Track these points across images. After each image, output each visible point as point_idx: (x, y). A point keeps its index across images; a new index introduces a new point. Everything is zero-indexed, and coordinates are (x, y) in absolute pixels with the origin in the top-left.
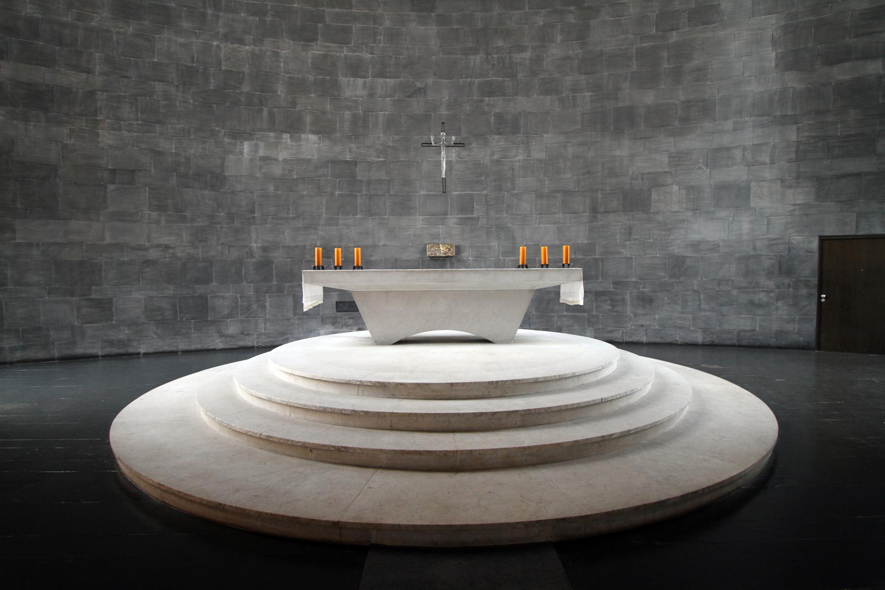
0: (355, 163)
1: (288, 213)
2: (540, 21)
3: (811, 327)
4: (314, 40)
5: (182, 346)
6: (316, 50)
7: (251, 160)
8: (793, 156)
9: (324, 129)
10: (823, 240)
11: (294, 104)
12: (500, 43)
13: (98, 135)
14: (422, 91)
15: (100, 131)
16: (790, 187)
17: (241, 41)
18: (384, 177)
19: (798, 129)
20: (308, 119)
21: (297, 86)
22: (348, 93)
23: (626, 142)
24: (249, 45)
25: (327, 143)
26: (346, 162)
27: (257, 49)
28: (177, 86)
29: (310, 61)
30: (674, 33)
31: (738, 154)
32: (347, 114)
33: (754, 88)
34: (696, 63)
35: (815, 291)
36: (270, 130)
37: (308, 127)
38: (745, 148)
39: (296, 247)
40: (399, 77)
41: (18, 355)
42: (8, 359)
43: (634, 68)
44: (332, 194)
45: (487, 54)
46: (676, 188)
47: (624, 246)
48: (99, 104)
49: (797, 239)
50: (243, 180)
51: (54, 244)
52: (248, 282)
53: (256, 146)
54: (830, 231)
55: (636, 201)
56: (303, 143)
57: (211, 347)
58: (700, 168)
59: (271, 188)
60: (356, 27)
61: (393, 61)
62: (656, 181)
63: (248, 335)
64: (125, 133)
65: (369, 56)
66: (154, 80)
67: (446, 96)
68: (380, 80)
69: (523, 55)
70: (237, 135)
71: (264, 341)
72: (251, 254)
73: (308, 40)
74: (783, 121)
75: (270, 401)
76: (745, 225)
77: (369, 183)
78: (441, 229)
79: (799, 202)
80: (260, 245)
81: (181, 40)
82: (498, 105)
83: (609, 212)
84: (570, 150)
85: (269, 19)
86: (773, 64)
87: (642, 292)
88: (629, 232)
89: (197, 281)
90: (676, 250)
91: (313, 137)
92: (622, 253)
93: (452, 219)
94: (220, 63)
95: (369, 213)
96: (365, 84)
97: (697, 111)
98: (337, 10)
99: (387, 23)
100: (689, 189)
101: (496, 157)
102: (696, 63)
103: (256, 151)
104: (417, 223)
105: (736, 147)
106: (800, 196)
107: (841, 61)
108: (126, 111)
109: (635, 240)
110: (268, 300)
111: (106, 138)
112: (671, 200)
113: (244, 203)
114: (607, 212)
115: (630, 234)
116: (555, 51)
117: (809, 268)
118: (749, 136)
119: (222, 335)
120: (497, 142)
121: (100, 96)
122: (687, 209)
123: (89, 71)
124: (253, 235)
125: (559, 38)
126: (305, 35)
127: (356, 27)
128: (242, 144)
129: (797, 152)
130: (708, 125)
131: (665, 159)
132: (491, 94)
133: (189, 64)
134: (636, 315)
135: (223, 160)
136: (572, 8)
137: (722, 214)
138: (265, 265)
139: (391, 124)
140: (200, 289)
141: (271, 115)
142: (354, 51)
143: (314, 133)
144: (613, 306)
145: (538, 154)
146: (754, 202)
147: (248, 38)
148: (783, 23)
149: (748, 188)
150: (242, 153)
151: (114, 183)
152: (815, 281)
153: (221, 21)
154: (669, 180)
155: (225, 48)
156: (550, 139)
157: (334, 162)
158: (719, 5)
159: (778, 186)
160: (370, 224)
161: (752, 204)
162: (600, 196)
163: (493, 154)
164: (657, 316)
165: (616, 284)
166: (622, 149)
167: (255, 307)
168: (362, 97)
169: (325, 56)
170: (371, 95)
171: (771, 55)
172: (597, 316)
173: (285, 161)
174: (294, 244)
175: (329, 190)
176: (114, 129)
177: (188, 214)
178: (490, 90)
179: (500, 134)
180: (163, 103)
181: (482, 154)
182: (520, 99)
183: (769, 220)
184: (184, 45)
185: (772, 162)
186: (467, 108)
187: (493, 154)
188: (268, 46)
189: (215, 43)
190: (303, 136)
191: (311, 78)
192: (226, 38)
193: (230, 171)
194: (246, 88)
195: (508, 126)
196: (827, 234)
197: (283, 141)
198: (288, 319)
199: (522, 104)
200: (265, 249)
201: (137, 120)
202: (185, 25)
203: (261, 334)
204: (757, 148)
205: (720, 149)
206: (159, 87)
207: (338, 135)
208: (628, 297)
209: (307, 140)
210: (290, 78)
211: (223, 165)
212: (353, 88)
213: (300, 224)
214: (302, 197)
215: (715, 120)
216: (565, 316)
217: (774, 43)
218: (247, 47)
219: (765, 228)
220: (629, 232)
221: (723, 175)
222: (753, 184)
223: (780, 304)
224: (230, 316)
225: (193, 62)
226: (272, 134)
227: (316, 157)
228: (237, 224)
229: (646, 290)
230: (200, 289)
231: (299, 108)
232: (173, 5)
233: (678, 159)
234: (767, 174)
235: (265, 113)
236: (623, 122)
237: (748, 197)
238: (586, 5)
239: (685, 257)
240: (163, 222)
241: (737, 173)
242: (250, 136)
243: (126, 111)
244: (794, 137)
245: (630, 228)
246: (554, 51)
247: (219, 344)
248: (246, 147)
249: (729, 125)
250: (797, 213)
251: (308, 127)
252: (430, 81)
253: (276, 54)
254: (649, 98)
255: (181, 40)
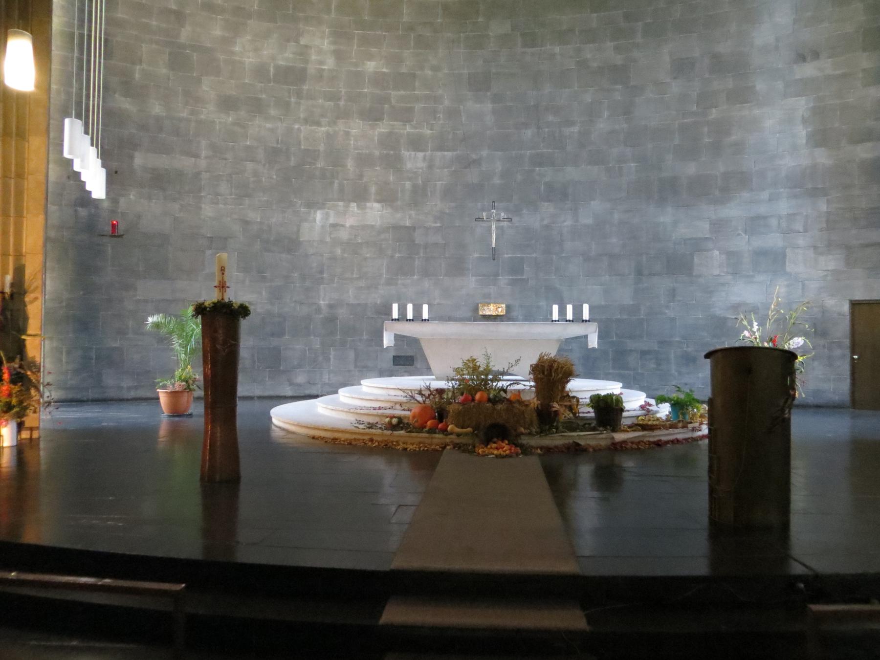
0: (414, 228)
1: (352, 274)
2: (588, 98)
3: (845, 386)
4: (380, 119)
5: (258, 392)
6: (383, 128)
7: (323, 227)
8: (825, 225)
9: (387, 198)
10: (855, 305)
11: (361, 176)
12: (551, 118)
13: (201, 208)
14: (477, 162)
15: (203, 206)
16: (821, 254)
17: (318, 124)
18: (441, 241)
19: (828, 200)
20: (373, 189)
21: (364, 160)
22: (409, 166)
23: (669, 210)
24: (325, 126)
25: (389, 210)
26: (406, 227)
27: (330, 129)
28: (264, 165)
29: (376, 138)
30: (714, 110)
31: (774, 222)
32: (408, 185)
33: (788, 163)
34: (733, 138)
35: (848, 352)
36: (339, 200)
37: (373, 197)
38: (780, 217)
39: (359, 304)
40: (456, 150)
41: (133, 394)
42: (125, 397)
43: (677, 141)
44: (392, 257)
45: (539, 128)
46: (716, 253)
47: (667, 307)
48: (203, 183)
49: (830, 302)
50: (315, 244)
51: (163, 300)
52: (315, 336)
53: (327, 214)
54: (859, 296)
55: (679, 263)
56: (368, 211)
57: (282, 394)
58: (739, 235)
59: (339, 251)
60: (418, 106)
61: (450, 137)
62: (697, 245)
63: (314, 384)
64: (221, 205)
65: (429, 132)
66: (247, 161)
67: (499, 166)
68: (439, 154)
69: (572, 129)
70: (311, 205)
71: (314, 392)
72: (319, 310)
73: (376, 120)
74: (814, 193)
75: (377, 400)
76: (780, 290)
77: (426, 247)
78: (492, 290)
79: (830, 268)
80: (327, 302)
81: (268, 125)
82: (548, 174)
83: (654, 275)
84: (616, 216)
85: (342, 103)
86: (804, 141)
87: (686, 351)
88: (673, 293)
89: (273, 335)
90: (718, 312)
91: (377, 205)
92: (666, 314)
93: (503, 280)
94: (299, 143)
95: (426, 273)
96: (424, 159)
97: (737, 182)
98: (402, 92)
99: (447, 102)
100: (730, 254)
101: (545, 222)
102: (733, 138)
103: (327, 219)
104: (470, 284)
105: (772, 216)
106: (831, 262)
107: (862, 141)
108: (224, 188)
109: (679, 301)
110: (332, 353)
111: (208, 210)
112: (712, 264)
113: (315, 265)
114: (652, 274)
115: (674, 296)
116: (602, 125)
117: (842, 330)
118: (784, 207)
119: (291, 384)
120: (547, 209)
121: (205, 176)
122: (728, 273)
123: (197, 156)
124: (322, 294)
125: (606, 114)
126: (373, 116)
127: (418, 106)
128: (315, 212)
129: (827, 221)
130: (746, 195)
131: (707, 226)
132: (540, 165)
133: (275, 146)
134: (680, 373)
135: (299, 226)
136: (619, 87)
137: (760, 278)
138: (331, 320)
139: (448, 193)
140: (275, 342)
141: (341, 190)
142: (416, 128)
143: (378, 202)
144: (659, 364)
145: (586, 219)
146: (790, 267)
147: (324, 121)
148: (812, 105)
149: (784, 256)
150: (315, 220)
151: (211, 249)
152: (847, 342)
153: (302, 108)
154: (710, 245)
155: (305, 130)
156: (597, 205)
157: (396, 228)
158: (754, 86)
159: (811, 253)
160: (427, 284)
161: (788, 269)
162: (644, 259)
163: (542, 220)
164: (700, 375)
165: (661, 343)
166: (666, 217)
167: (320, 358)
168: (422, 168)
169: (390, 134)
170: (430, 167)
171: (802, 133)
172: (642, 374)
173: (352, 227)
174: (356, 302)
175: (389, 252)
176: (213, 203)
177: (267, 275)
178: (540, 161)
179: (549, 201)
180: (252, 179)
181: (534, 220)
182: (569, 169)
183: (803, 285)
184: (272, 130)
185: (806, 231)
186: (519, 177)
187: (542, 220)
188: (341, 126)
189: (297, 127)
190: (368, 204)
191: (377, 153)
192: (306, 121)
193: (304, 237)
194: (320, 164)
195: (559, 194)
196: (857, 298)
197: (351, 209)
198: (349, 371)
199: (572, 173)
200: (331, 306)
201: (231, 195)
202: (273, 112)
203: (325, 384)
204: (791, 217)
205: (759, 217)
206: (250, 166)
207: (399, 203)
208: (672, 356)
209: (372, 208)
210: (358, 153)
211: (298, 231)
212: (414, 161)
213: (362, 283)
214: (366, 259)
215: (752, 190)
216: (610, 374)
217: (804, 121)
218: (323, 129)
219: (800, 291)
220: (673, 293)
221: (758, 242)
222: (788, 250)
223: (816, 363)
224: (300, 366)
225: (278, 143)
226: (341, 204)
227: (378, 224)
228: (308, 284)
229: (690, 349)
230: (275, 342)
231: (365, 179)
232: (264, 96)
233: (719, 226)
234: (801, 242)
235: (336, 185)
236: (668, 191)
237: (784, 263)
238: (632, 84)
239: (726, 319)
240: (247, 282)
241: (773, 240)
242: (322, 206)
243: (224, 188)
244: (823, 207)
245: (674, 290)
246: (602, 126)
247: (289, 392)
248: (319, 215)
249: (765, 195)
250: (829, 278)
251: (373, 197)
252: (485, 153)
253: (347, 134)
254: (691, 169)
255: (268, 125)
